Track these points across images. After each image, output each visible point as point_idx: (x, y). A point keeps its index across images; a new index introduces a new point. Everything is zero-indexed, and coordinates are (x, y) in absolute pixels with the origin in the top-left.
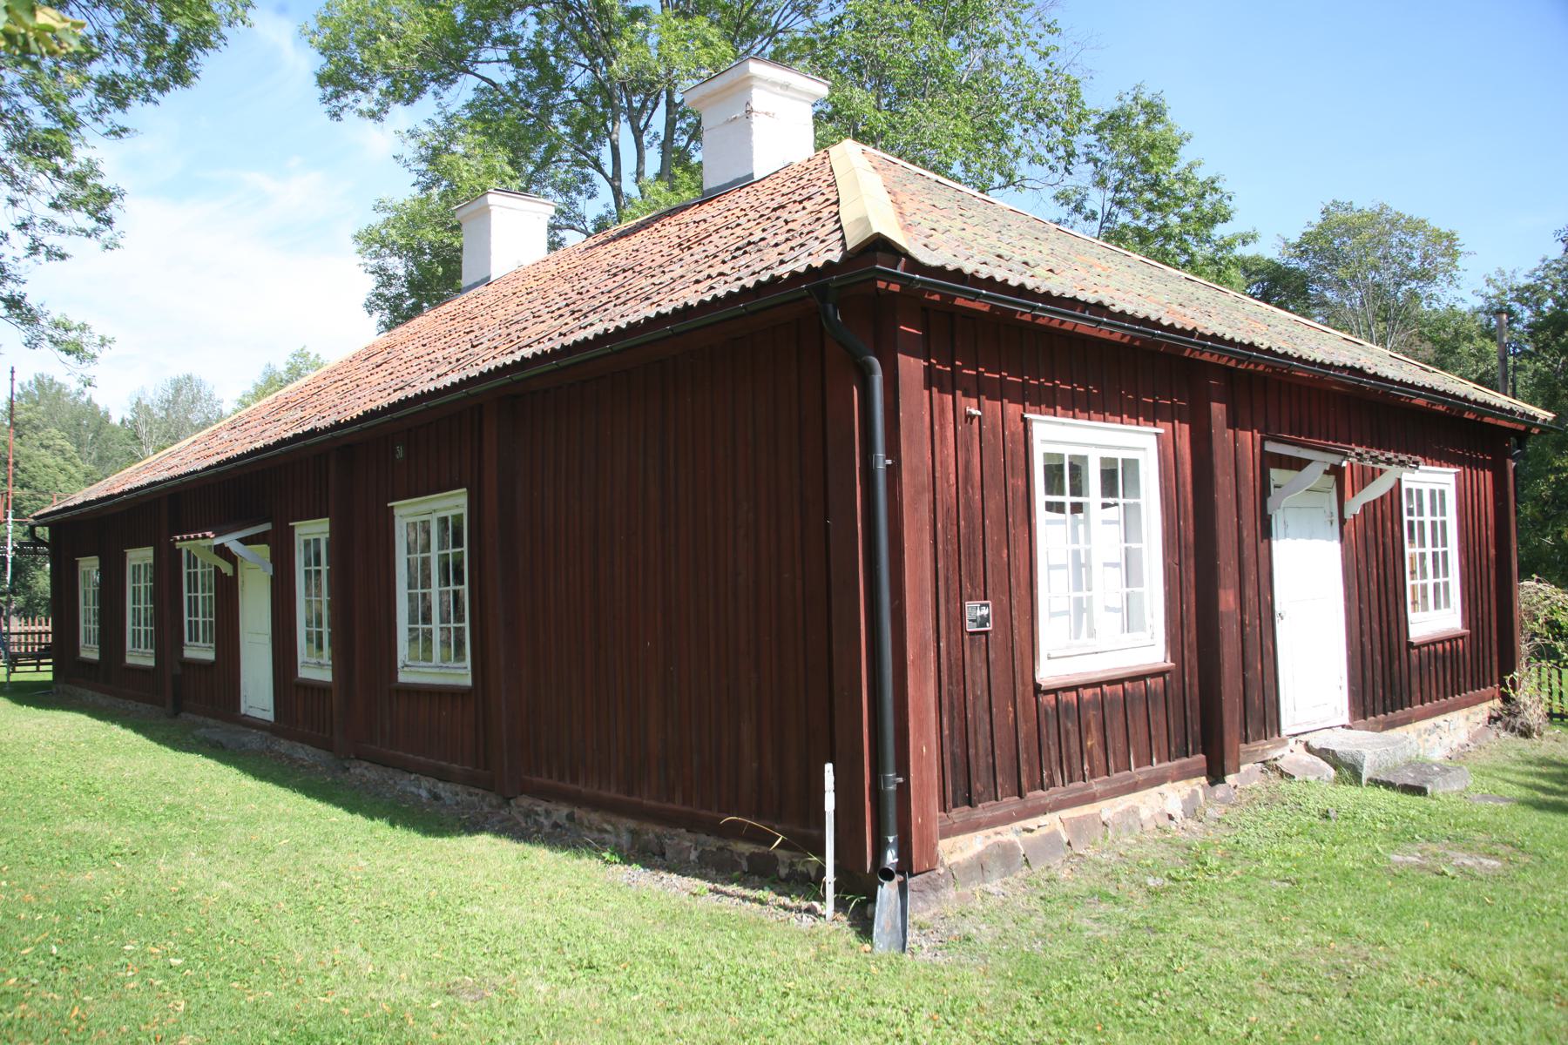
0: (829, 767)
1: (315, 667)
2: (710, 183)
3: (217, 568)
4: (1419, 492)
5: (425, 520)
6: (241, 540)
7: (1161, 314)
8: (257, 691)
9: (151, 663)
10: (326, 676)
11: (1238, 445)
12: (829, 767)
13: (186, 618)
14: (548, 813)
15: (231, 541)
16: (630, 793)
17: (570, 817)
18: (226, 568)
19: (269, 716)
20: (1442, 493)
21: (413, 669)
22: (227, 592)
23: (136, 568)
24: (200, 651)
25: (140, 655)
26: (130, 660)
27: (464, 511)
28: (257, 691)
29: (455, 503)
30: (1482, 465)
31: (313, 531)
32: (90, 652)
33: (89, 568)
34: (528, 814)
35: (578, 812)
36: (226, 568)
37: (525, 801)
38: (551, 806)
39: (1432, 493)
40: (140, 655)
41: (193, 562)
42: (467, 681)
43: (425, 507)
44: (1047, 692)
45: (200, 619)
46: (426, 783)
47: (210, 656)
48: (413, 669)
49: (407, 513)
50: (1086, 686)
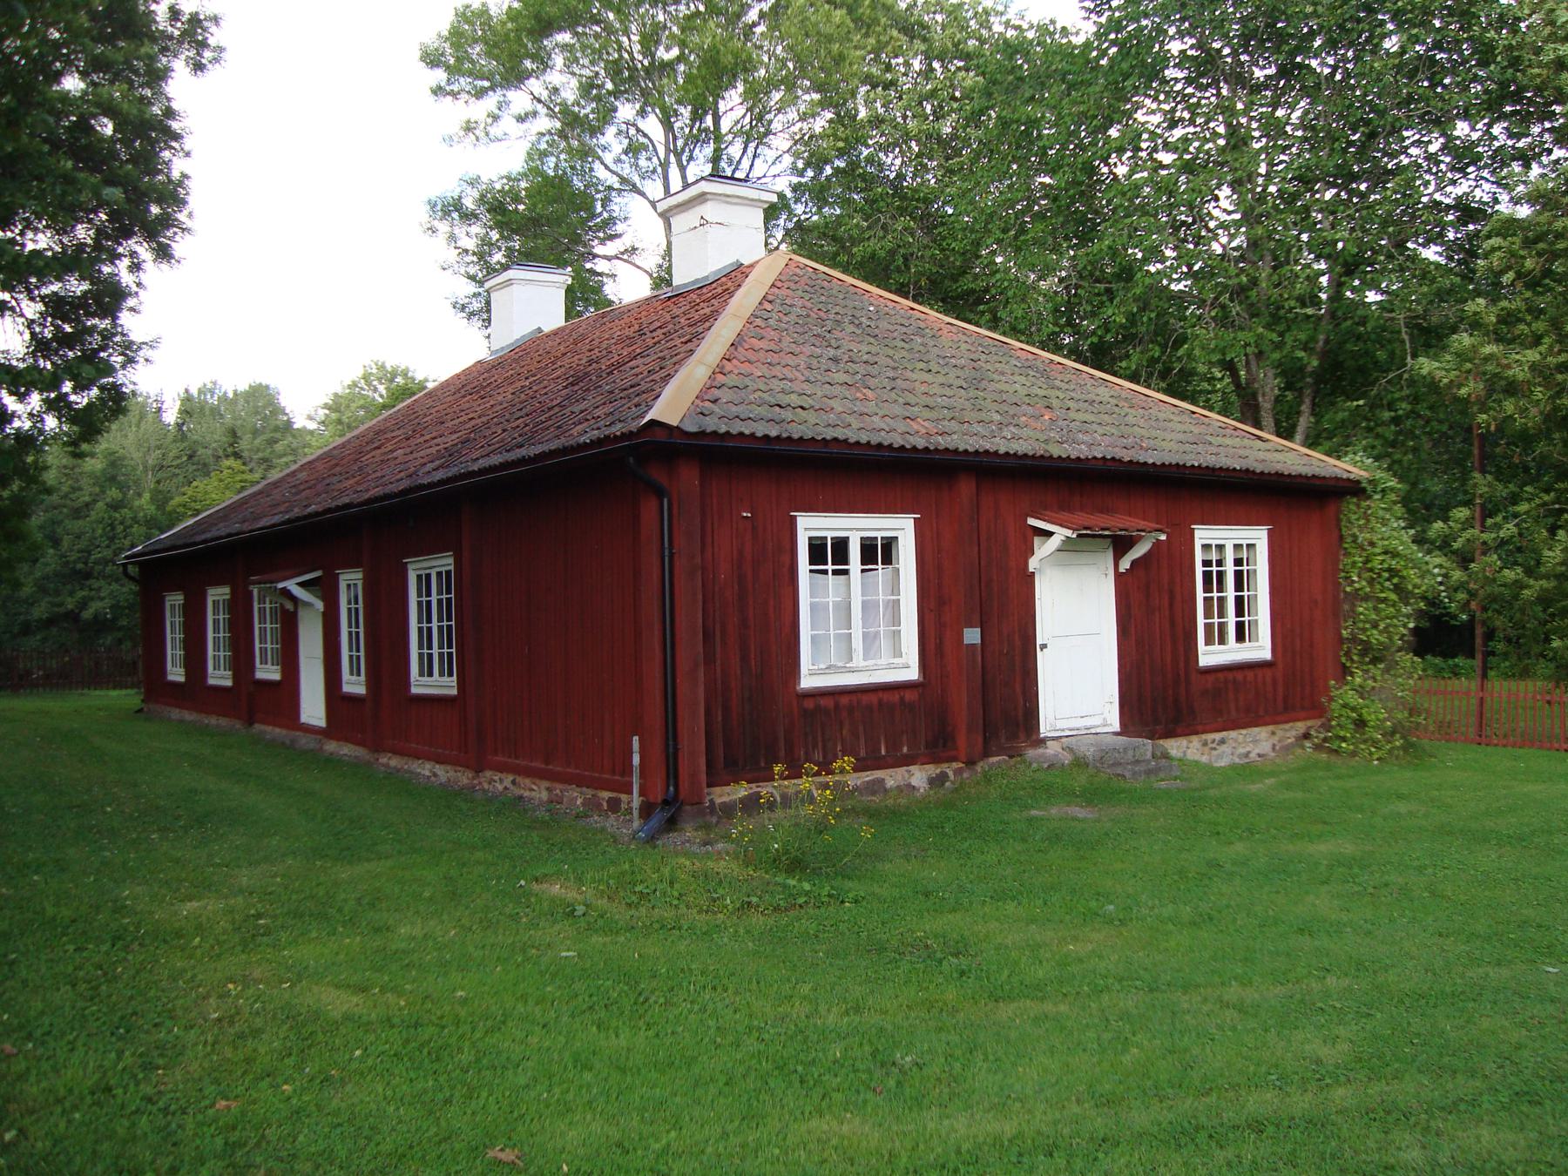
0: (636, 739)
1: (355, 685)
4: (441, 674)
5: (427, 575)
6: (300, 584)
8: (313, 709)
9: (229, 683)
10: (361, 690)
12: (636, 739)
13: (257, 645)
14: (501, 780)
15: (292, 585)
16: (547, 763)
17: (513, 782)
18: (289, 606)
19: (322, 723)
20: (421, 674)
21: (420, 685)
24: (268, 672)
25: (219, 676)
26: (211, 682)
27: (452, 568)
28: (313, 709)
29: (446, 562)
31: (350, 580)
32: (176, 673)
33: (174, 600)
35: (519, 779)
36: (289, 606)
37: (488, 774)
38: (503, 776)
39: (430, 674)
40: (219, 676)
42: (454, 692)
43: (425, 564)
45: (268, 626)
46: (428, 765)
47: (276, 676)
48: (420, 685)
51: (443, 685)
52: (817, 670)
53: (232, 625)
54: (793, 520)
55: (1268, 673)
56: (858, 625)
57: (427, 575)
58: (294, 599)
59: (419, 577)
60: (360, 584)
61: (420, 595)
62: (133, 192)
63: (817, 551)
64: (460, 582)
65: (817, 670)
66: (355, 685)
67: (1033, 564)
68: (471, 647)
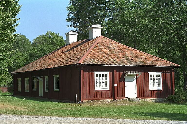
1: (47, 91)
2: (90, 38)
3: (37, 81)
5: (56, 76)
7: (23, 34)
11: (118, 75)
20: (55, 89)
22: (38, 83)
23: (56, 78)
24: (35, 89)
28: (41, 93)
29: (58, 76)
30: (169, 73)
31: (47, 77)
34: (62, 101)
36: (38, 81)
39: (56, 89)
41: (34, 79)
44: (95, 91)
48: (55, 90)
49: (55, 76)
50: (100, 91)
51: (58, 90)
52: (97, 88)
53: (29, 83)
54: (17, 79)
55: (161, 91)
56: (101, 83)
57: (56, 76)
58: (39, 80)
59: (55, 77)
60: (46, 90)
61: (55, 80)
62: (28, 40)
63: (97, 76)
64: (60, 78)
65: (97, 88)
66: (47, 91)
67: (125, 77)
68: (61, 86)
